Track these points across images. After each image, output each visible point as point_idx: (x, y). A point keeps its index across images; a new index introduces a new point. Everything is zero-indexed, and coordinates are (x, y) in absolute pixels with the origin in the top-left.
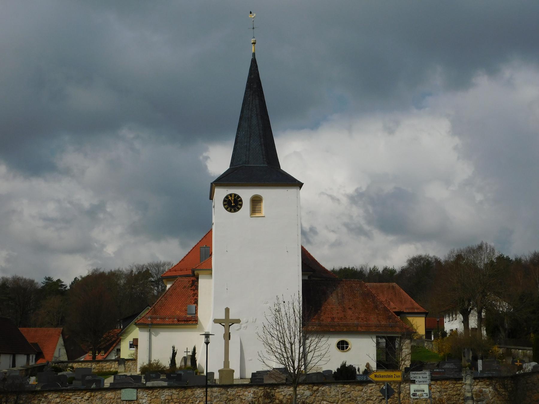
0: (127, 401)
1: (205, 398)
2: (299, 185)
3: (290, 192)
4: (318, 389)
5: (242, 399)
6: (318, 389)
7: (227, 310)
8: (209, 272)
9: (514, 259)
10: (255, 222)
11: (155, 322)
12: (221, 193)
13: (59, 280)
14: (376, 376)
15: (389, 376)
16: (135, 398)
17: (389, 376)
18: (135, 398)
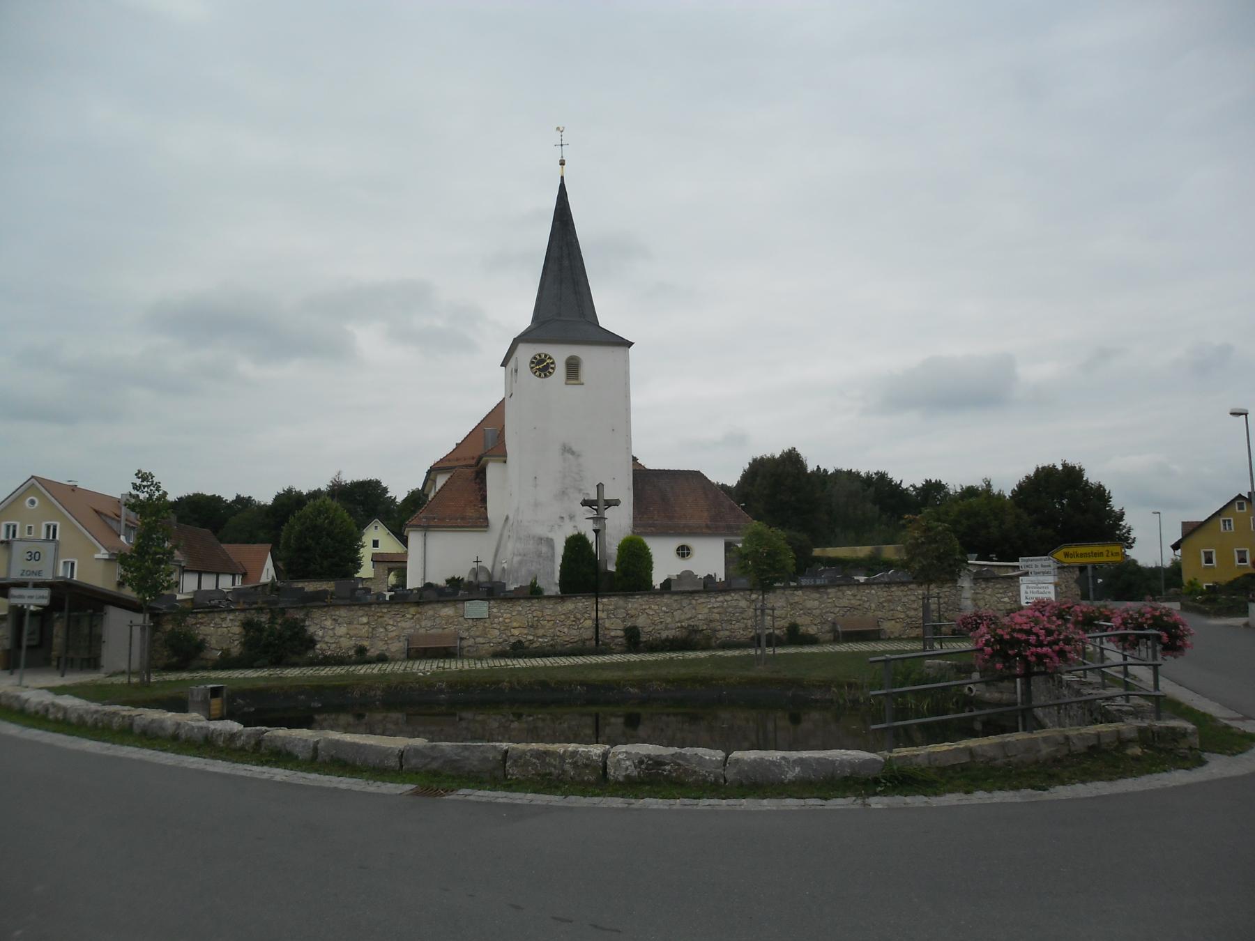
2: (630, 344)
7: (600, 487)
10: (573, 390)
11: (432, 523)
12: (527, 353)
13: (238, 497)
14: (1066, 555)
15: (1095, 555)
17: (1095, 555)
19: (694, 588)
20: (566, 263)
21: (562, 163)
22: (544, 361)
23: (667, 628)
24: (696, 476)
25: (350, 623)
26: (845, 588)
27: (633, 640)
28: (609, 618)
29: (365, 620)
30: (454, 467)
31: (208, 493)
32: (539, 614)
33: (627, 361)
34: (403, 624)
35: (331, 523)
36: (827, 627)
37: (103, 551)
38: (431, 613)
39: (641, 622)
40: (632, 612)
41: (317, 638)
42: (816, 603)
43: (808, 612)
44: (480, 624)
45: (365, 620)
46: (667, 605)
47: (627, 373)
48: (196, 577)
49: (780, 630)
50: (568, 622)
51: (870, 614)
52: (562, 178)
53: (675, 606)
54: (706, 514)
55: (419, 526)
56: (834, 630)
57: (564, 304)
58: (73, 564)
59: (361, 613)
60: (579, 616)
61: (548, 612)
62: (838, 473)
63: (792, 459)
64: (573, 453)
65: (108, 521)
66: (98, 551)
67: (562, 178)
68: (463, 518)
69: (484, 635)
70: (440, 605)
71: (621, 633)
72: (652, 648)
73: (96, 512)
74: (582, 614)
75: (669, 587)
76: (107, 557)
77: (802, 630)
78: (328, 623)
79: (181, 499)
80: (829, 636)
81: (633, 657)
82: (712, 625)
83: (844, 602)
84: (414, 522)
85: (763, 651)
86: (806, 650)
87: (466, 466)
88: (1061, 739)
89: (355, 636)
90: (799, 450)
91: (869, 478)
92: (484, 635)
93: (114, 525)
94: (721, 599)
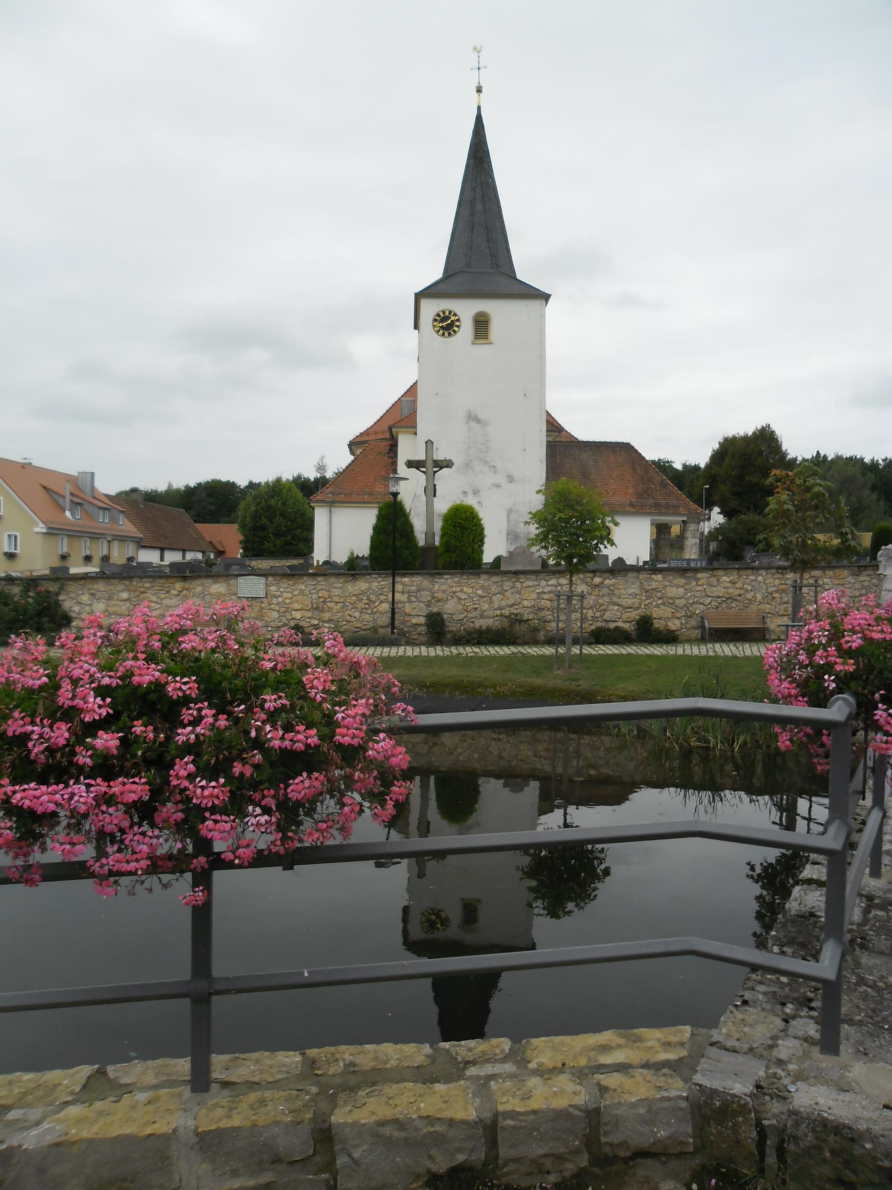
0: (248, 598)
1: (390, 595)
2: (546, 297)
3: (533, 305)
4: (602, 583)
5: (460, 599)
6: (602, 583)
8: (413, 430)
9: (784, 449)
10: (482, 350)
11: (338, 499)
12: (430, 308)
16: (262, 594)
18: (262, 594)
19: (530, 568)
20: (479, 206)
21: (479, 90)
22: (448, 318)
23: (482, 616)
24: (626, 449)
25: (110, 599)
26: (720, 573)
27: (437, 630)
28: (410, 601)
29: (125, 595)
30: (366, 442)
31: (224, 479)
32: (326, 594)
33: (542, 317)
34: (167, 602)
35: (284, 503)
36: (693, 622)
37: (42, 525)
38: (199, 589)
39: (450, 608)
40: (439, 595)
41: (73, 615)
42: (681, 590)
43: (669, 602)
44: (256, 605)
45: (125, 595)
46: (483, 587)
47: (542, 331)
48: (181, 553)
49: (625, 622)
50: (360, 605)
51: (754, 607)
52: (479, 108)
53: (494, 589)
54: (631, 491)
55: (324, 501)
56: (702, 627)
57: (480, 258)
58: (16, 537)
59: (120, 587)
60: (373, 598)
61: (337, 592)
62: (838, 458)
63: (765, 441)
64: (479, 421)
65: (56, 497)
66: (37, 525)
67: (479, 108)
68: (370, 494)
69: (260, 617)
70: (210, 581)
71: (422, 620)
72: (458, 641)
73: (44, 487)
74: (377, 596)
75: (499, 567)
76: (45, 531)
77: (657, 624)
78: (85, 598)
79: (199, 484)
80: (697, 633)
81: (438, 651)
82: (542, 614)
83: (719, 591)
84: (319, 497)
85: (569, 650)
86: (657, 650)
87: (383, 439)
88: (298, 1143)
89: (115, 613)
90: (774, 427)
91: (874, 465)
92: (260, 617)
93: (61, 500)
94: (553, 582)
